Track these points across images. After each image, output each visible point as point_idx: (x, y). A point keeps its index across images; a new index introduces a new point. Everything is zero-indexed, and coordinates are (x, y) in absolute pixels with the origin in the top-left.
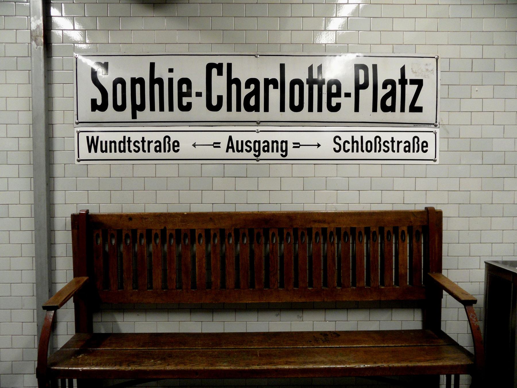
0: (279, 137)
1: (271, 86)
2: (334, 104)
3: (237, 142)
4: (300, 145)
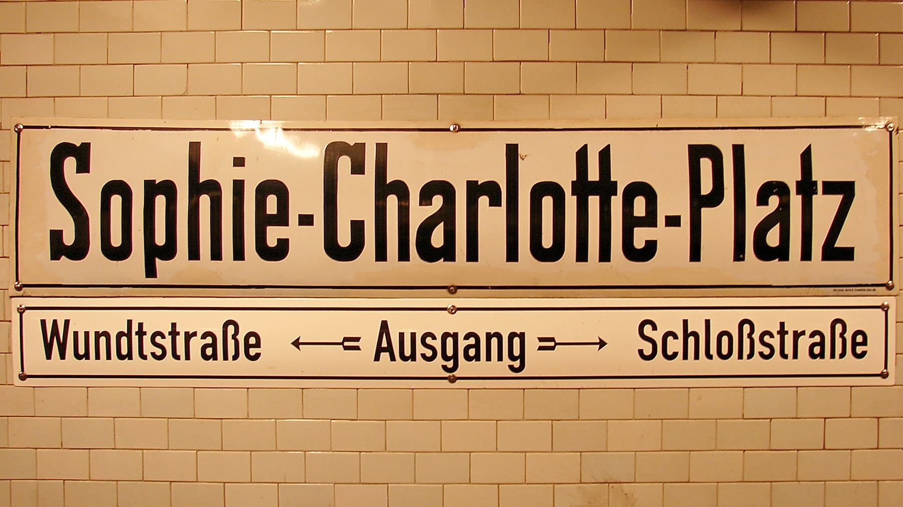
0: (505, 324)
1: (483, 201)
2: (639, 243)
3: (402, 335)
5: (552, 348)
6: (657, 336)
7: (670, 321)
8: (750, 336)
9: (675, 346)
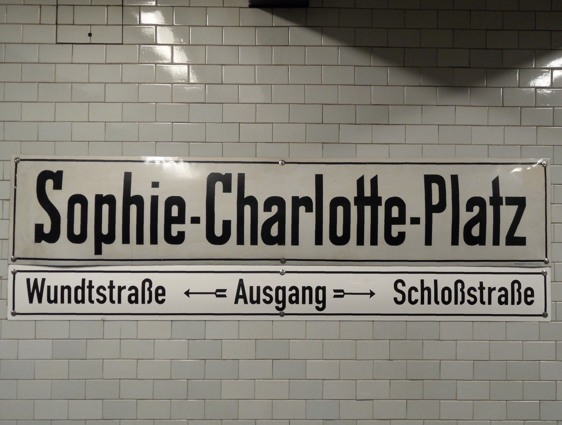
0: (314, 281)
1: (302, 209)
2: (395, 234)
3: (251, 288)
5: (342, 296)
6: (406, 290)
7: (412, 281)
8: (462, 290)
9: (416, 296)
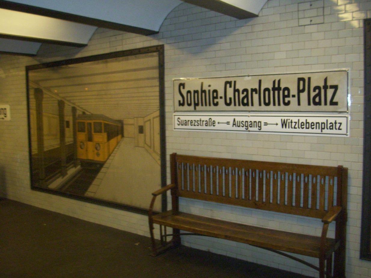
0: (257, 119)
1: (254, 93)
2: (286, 101)
3: (238, 121)
4: (268, 124)
